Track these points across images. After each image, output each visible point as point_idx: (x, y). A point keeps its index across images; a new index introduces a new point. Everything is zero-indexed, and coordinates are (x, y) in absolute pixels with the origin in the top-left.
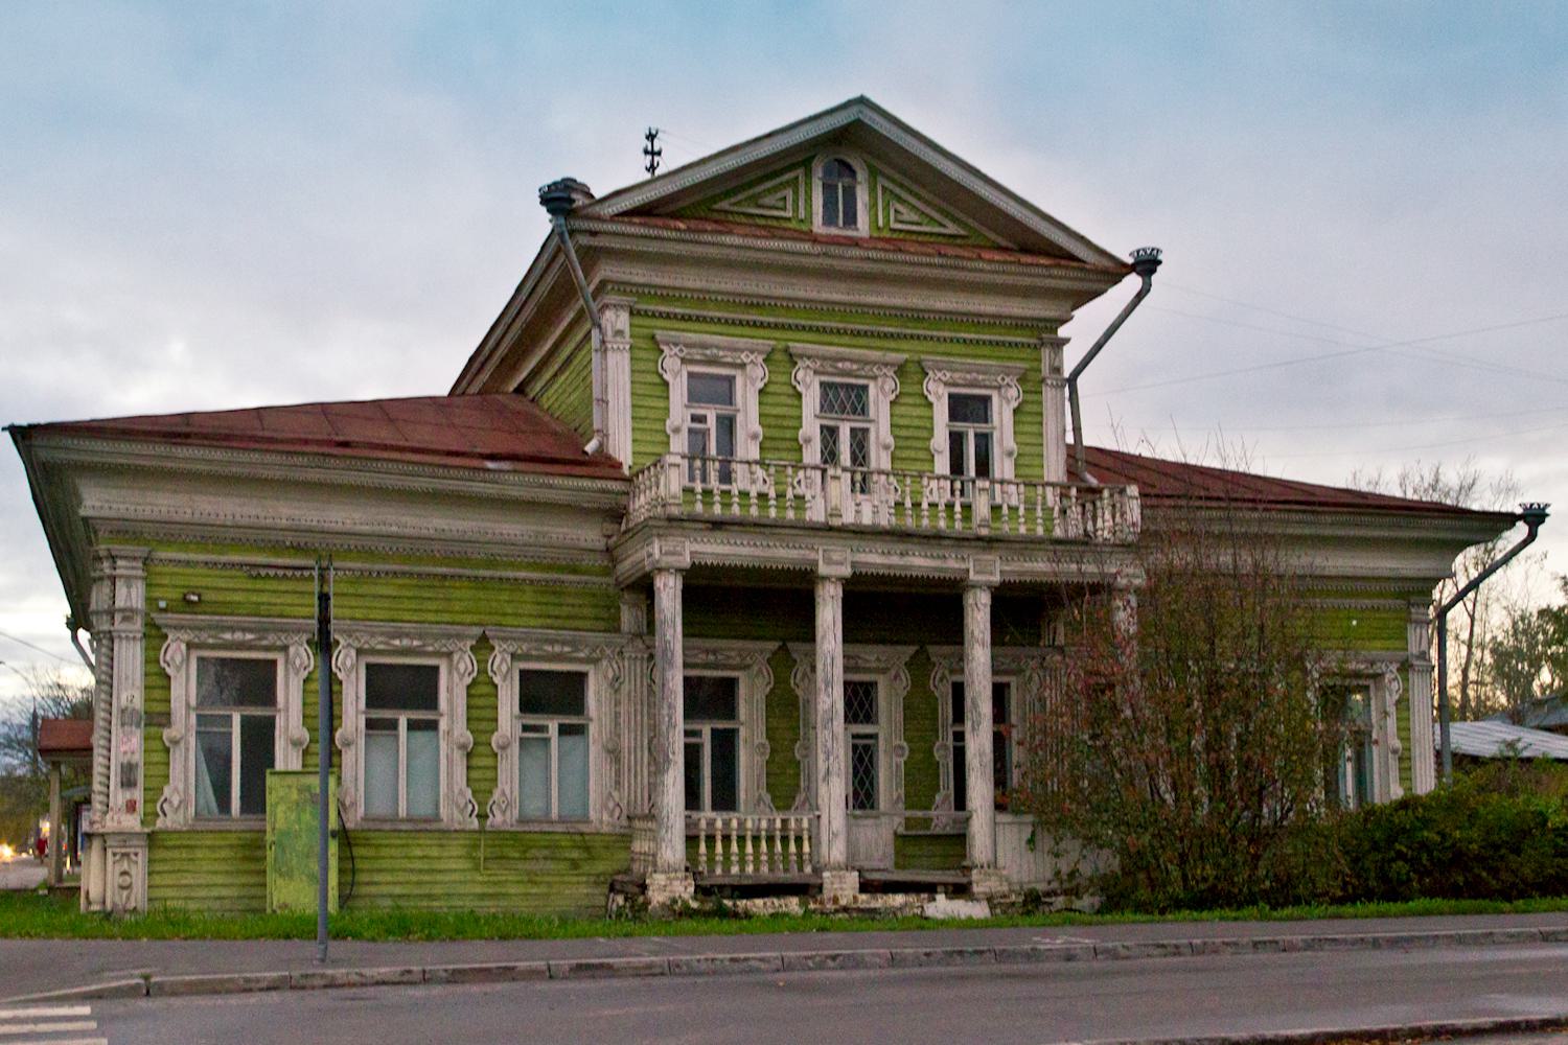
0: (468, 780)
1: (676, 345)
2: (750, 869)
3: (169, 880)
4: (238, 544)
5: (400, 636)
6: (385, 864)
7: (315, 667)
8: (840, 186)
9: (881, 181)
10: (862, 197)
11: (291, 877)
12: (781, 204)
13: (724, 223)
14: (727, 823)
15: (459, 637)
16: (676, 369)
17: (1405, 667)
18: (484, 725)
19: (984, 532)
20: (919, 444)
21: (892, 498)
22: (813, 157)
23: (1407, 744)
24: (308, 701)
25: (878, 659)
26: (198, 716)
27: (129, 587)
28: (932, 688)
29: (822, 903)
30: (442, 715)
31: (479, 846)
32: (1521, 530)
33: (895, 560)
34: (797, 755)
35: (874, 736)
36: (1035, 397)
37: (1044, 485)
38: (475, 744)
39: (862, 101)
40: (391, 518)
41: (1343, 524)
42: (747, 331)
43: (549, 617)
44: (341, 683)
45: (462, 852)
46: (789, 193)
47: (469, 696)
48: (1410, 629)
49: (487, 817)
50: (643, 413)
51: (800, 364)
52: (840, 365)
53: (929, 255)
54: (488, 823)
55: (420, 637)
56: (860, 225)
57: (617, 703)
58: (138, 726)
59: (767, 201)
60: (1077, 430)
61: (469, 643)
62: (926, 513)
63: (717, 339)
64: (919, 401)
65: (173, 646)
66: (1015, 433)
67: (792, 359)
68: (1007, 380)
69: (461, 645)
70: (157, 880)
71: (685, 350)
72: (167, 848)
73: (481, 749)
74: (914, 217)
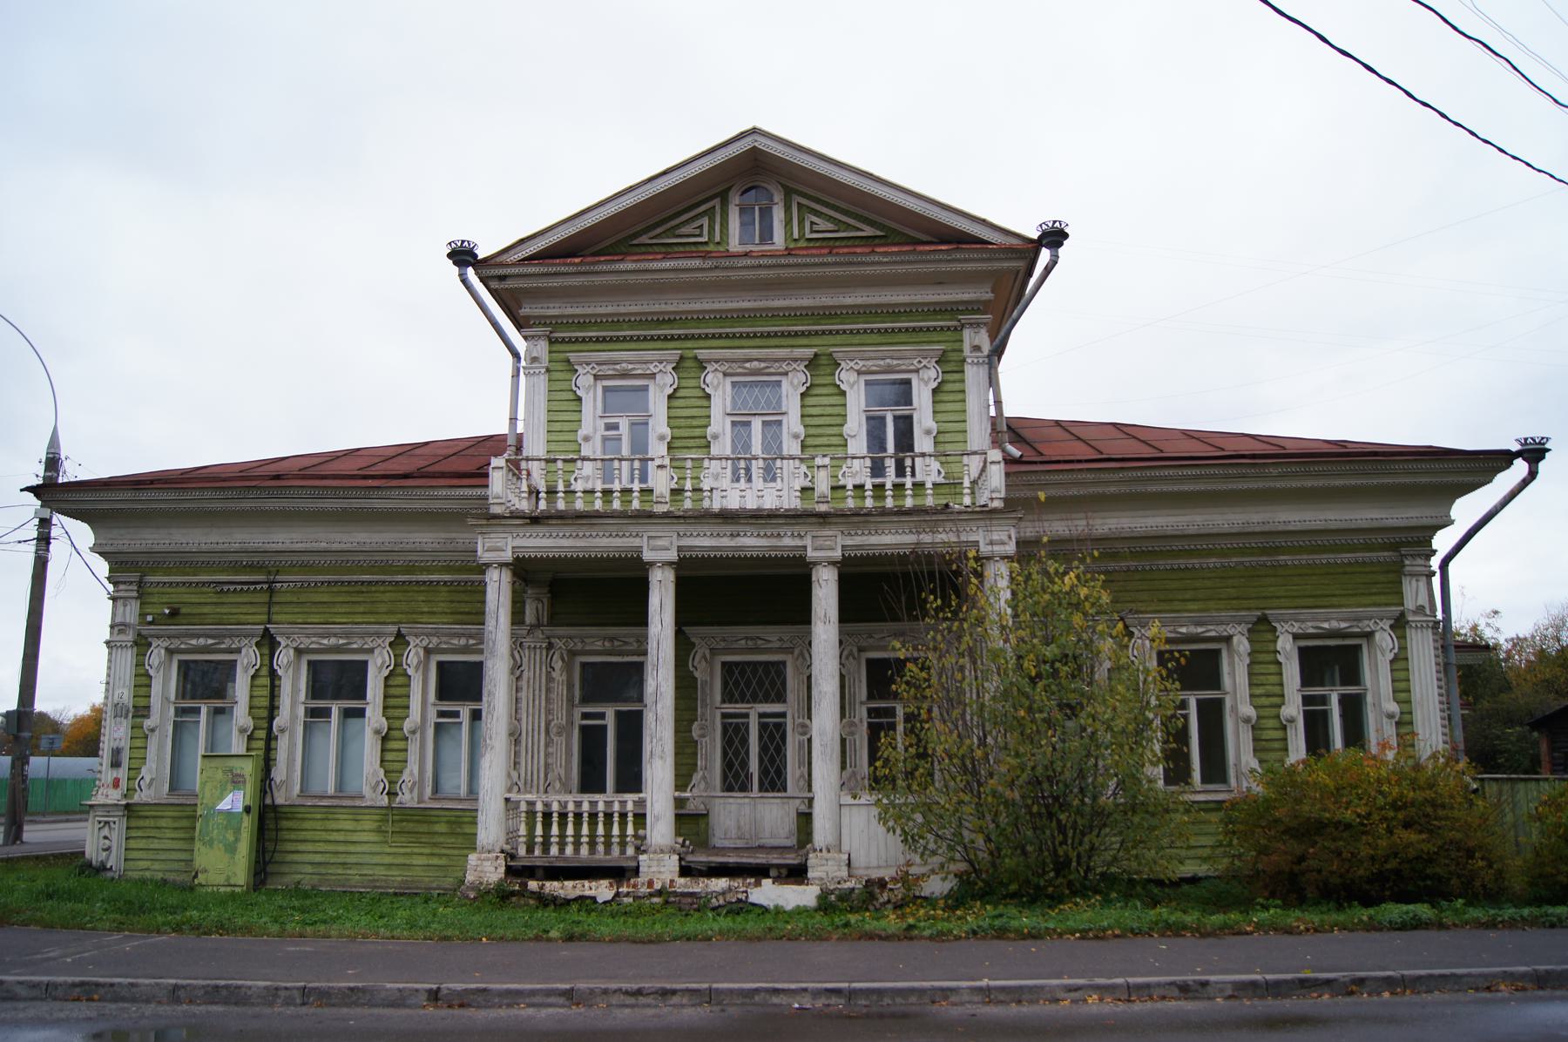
0: (382, 761)
1: (588, 364)
2: (569, 850)
3: (142, 844)
4: (208, 567)
5: (328, 636)
6: (309, 835)
7: (261, 665)
8: (757, 208)
9: (797, 199)
10: (778, 214)
11: (211, 845)
12: (697, 232)
13: (647, 250)
14: (593, 804)
15: (379, 635)
16: (852, 380)
17: (1400, 624)
18: (397, 713)
19: (823, 508)
20: (835, 430)
21: (799, 483)
22: (729, 189)
23: (1406, 708)
24: (255, 694)
25: (781, 640)
26: (176, 709)
27: (125, 606)
28: (691, 669)
29: (635, 886)
30: (304, 703)
31: (388, 821)
32: (1520, 468)
33: (726, 542)
34: (694, 734)
35: (783, 715)
36: (956, 376)
37: (620, 460)
38: (389, 729)
39: (754, 131)
40: (338, 537)
41: (1294, 475)
42: (659, 344)
43: (461, 613)
44: (280, 678)
45: (374, 825)
46: (705, 221)
47: (386, 686)
48: (1406, 581)
49: (397, 794)
50: (557, 426)
51: (710, 368)
52: (748, 365)
53: (823, 255)
54: (398, 800)
55: (347, 635)
56: (776, 239)
57: (518, 690)
58: (126, 717)
59: (684, 230)
60: (998, 403)
61: (255, 640)
62: (929, 492)
63: (755, 353)
64: (835, 391)
65: (156, 651)
66: (934, 412)
67: (701, 365)
68: (924, 362)
69: (380, 641)
70: (133, 844)
71: (597, 368)
72: (140, 817)
73: (395, 733)
74: (830, 226)
